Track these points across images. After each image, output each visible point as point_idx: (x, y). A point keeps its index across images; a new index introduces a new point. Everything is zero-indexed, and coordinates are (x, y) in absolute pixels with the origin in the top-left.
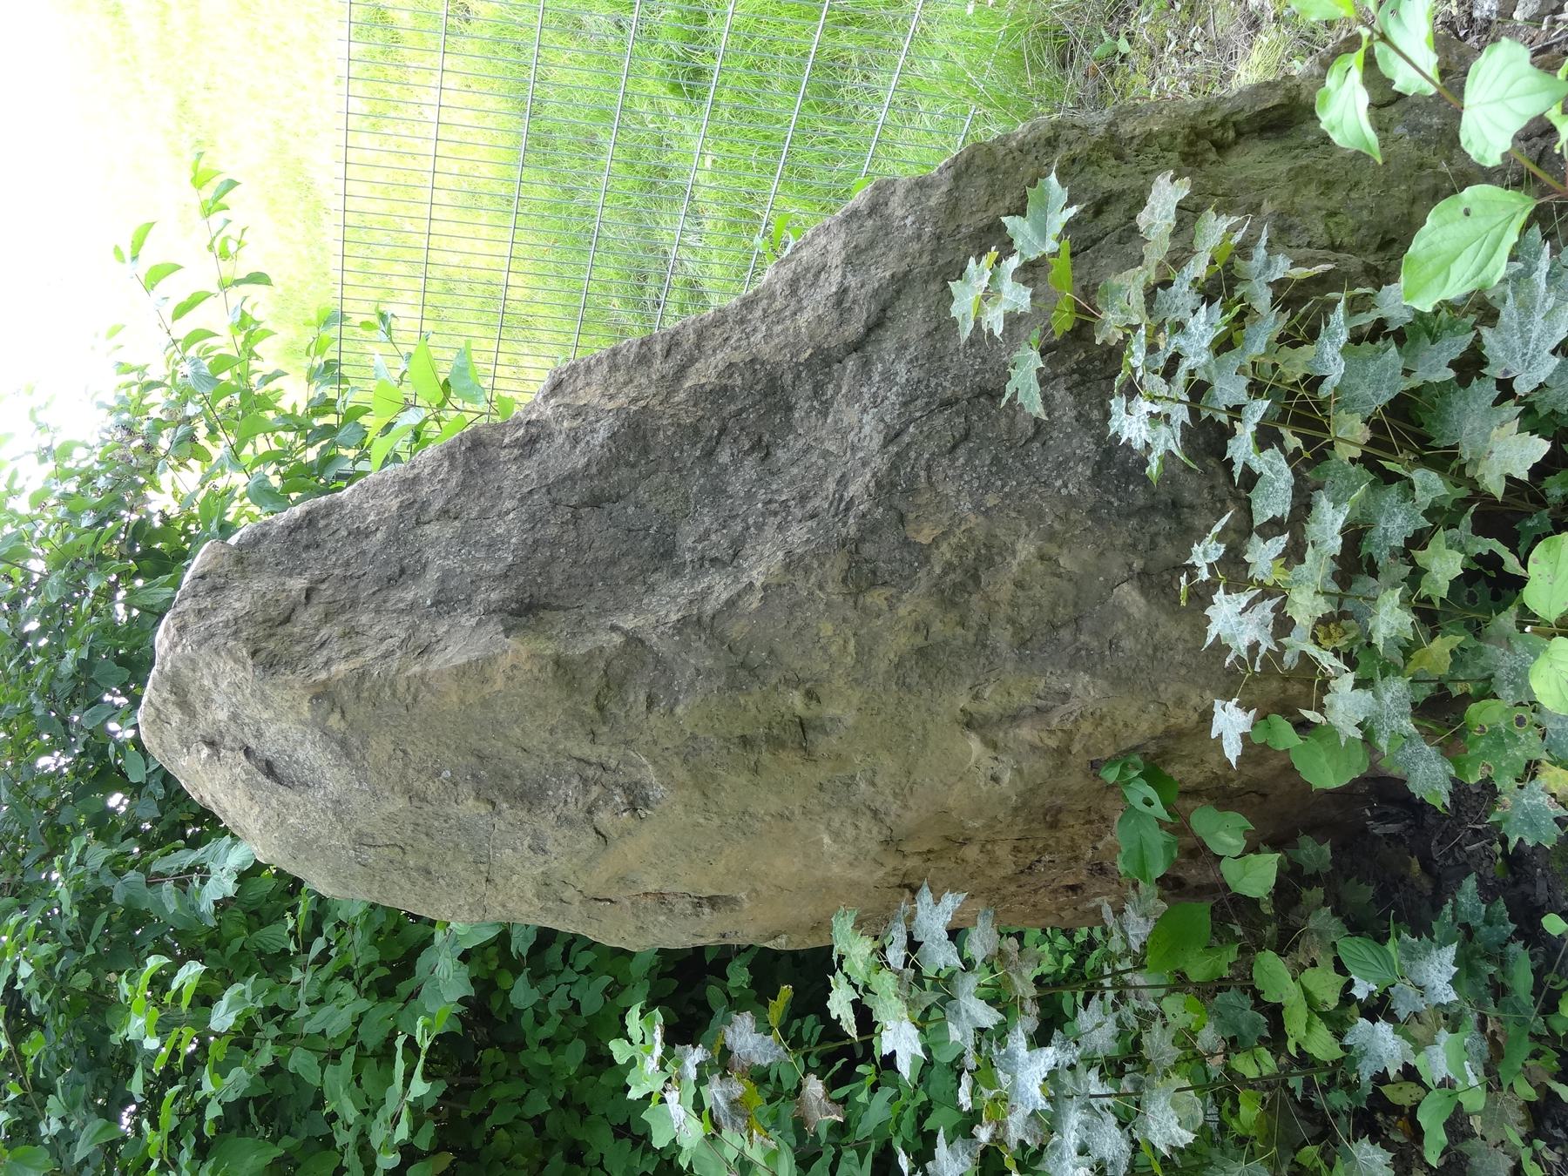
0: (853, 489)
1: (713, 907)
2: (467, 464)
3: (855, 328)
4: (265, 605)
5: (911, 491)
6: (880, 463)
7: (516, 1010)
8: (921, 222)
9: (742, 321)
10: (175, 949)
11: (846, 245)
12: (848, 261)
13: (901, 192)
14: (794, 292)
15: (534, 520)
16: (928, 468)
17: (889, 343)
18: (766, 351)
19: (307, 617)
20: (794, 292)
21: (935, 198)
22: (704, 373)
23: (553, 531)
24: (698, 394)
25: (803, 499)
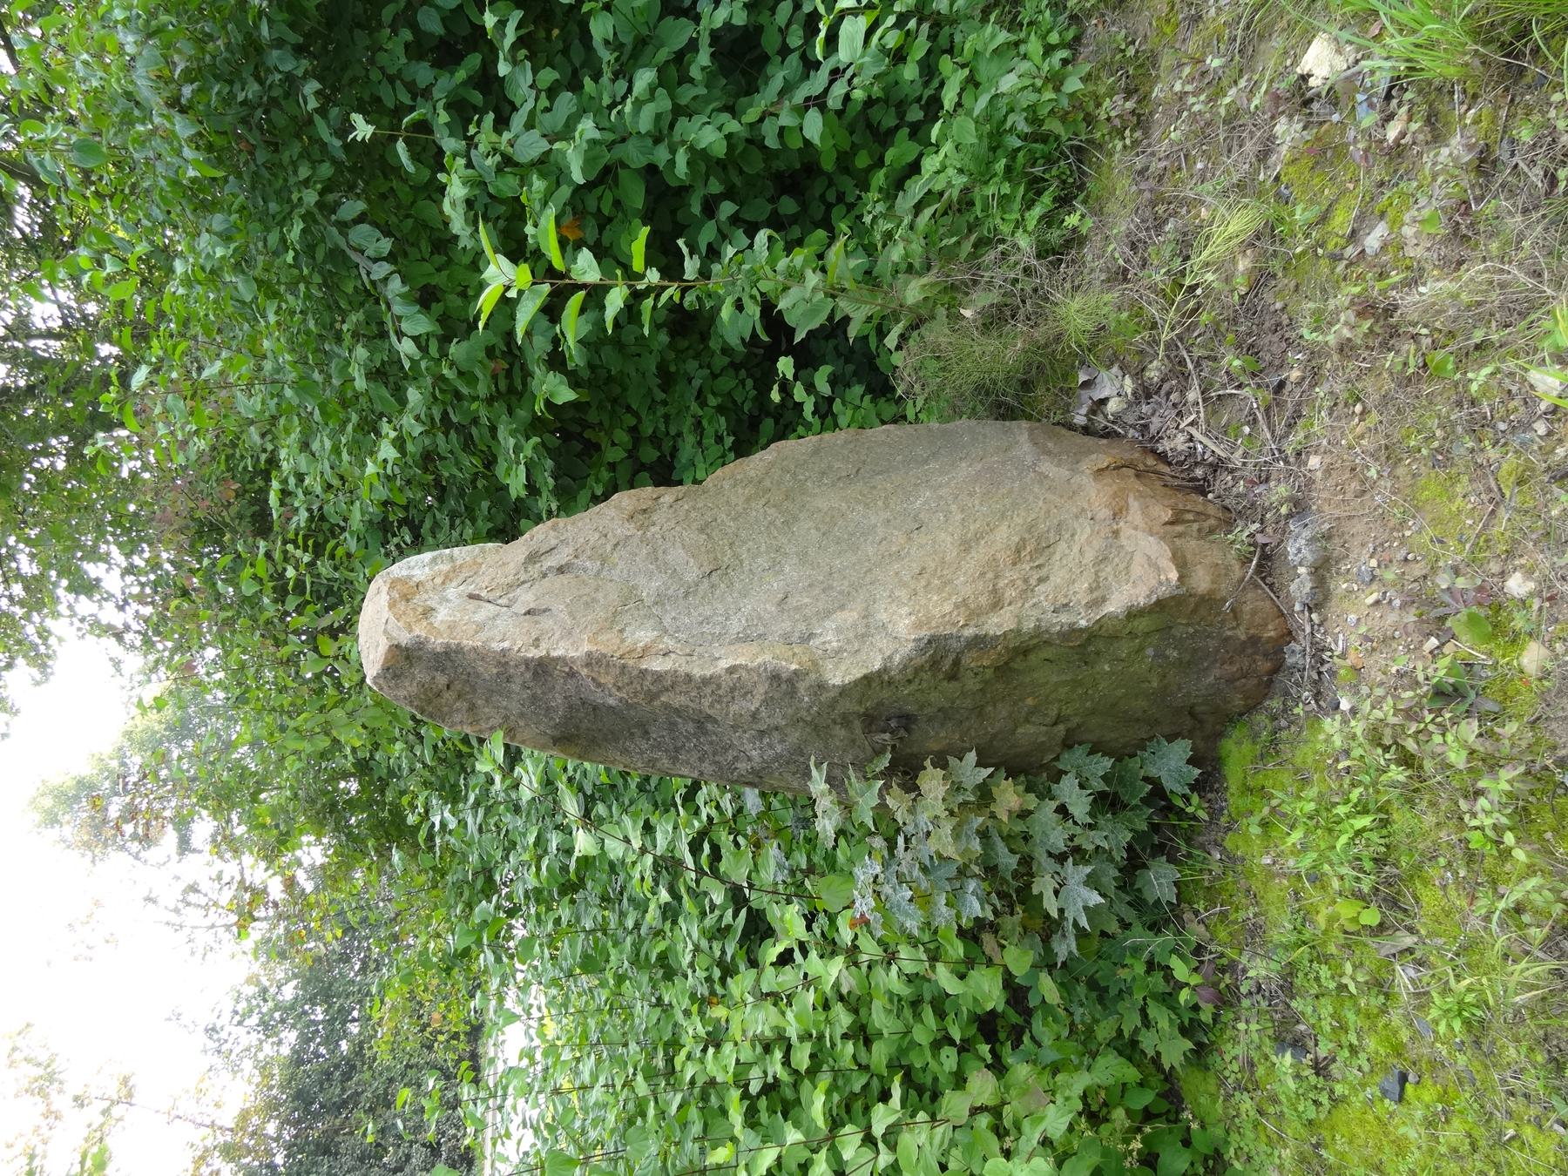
22: (678, 700)
24: (666, 706)
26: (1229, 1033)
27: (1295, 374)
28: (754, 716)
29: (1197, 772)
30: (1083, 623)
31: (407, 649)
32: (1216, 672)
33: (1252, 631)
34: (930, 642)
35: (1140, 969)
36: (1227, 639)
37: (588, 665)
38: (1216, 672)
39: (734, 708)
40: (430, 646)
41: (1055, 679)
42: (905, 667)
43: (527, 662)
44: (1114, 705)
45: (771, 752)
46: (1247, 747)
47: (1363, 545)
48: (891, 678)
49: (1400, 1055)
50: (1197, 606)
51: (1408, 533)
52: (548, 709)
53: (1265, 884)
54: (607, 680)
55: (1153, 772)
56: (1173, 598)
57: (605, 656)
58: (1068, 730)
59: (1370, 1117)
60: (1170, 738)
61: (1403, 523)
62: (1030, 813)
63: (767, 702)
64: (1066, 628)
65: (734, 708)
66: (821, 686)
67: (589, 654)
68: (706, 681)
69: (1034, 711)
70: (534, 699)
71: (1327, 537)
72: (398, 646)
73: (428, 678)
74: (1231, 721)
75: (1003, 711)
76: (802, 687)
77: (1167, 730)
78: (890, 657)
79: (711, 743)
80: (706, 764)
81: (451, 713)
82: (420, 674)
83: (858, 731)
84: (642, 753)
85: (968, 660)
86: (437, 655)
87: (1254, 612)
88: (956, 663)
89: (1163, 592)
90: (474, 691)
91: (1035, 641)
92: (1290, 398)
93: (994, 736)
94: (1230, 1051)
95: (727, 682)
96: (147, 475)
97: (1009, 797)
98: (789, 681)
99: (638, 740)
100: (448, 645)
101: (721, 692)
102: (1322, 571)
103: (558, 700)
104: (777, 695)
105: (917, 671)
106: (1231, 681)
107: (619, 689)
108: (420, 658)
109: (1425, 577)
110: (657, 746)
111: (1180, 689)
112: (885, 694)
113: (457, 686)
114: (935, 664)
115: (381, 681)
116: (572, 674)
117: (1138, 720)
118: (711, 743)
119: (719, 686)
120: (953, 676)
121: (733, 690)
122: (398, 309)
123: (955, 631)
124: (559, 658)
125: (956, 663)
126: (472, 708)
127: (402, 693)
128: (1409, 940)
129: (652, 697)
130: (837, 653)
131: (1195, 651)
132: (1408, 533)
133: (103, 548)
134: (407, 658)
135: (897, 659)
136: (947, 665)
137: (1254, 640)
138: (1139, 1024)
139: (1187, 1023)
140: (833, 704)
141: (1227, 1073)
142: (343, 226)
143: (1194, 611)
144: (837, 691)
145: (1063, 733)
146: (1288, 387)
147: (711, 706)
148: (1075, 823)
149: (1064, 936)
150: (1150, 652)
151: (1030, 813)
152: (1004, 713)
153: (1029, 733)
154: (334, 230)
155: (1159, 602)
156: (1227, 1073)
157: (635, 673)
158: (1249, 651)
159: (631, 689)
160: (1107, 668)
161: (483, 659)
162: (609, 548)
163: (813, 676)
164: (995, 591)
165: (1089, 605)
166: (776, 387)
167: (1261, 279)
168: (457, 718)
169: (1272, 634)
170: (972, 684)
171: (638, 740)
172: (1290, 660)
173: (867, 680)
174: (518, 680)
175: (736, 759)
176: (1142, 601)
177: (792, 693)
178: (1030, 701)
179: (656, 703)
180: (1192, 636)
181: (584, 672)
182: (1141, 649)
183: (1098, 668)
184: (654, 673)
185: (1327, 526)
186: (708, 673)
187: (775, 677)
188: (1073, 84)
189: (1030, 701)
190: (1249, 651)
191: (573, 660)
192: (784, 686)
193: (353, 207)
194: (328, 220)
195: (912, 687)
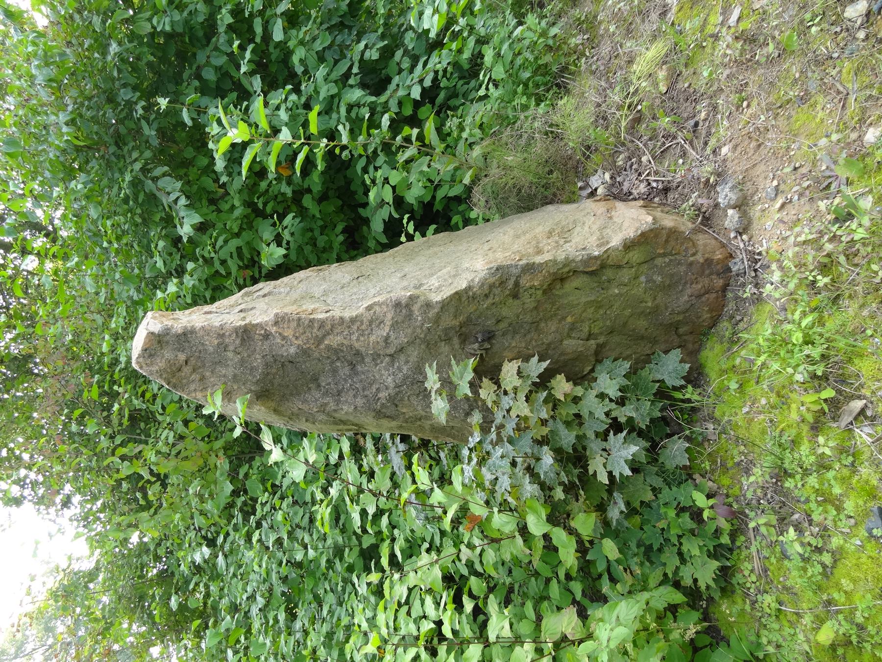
0: (380, 395)
1: (137, 459)
2: (242, 336)
3: (391, 351)
4: (171, 365)
5: (402, 400)
6: (391, 391)
7: (699, 508)
8: (424, 320)
9: (349, 327)
10: (176, 60)
11: (393, 318)
12: (392, 326)
13: (419, 304)
14: (370, 325)
15: (267, 365)
16: (409, 397)
17: (402, 358)
18: (357, 345)
19: (187, 370)
20: (370, 325)
21: (432, 313)
22: (334, 340)
23: (274, 371)
24: (329, 348)
25: (364, 390)
26: (744, 553)
27: (703, 115)
28: (386, 339)
29: (688, 366)
30: (596, 253)
31: (159, 335)
32: (689, 291)
33: (706, 256)
34: (497, 269)
35: (672, 513)
36: (691, 264)
37: (276, 323)
38: (689, 291)
39: (373, 338)
40: (173, 331)
41: (584, 300)
42: (483, 285)
43: (236, 330)
44: (625, 324)
45: (400, 375)
46: (718, 348)
47: (766, 178)
48: (474, 294)
49: (875, 497)
50: (668, 237)
51: (792, 153)
52: (252, 369)
53: (747, 429)
54: (288, 333)
55: (659, 377)
56: (651, 230)
57: (286, 314)
58: (598, 345)
59: (864, 559)
60: (666, 352)
61: (788, 148)
62: (580, 399)
63: (395, 326)
64: (586, 257)
65: (373, 338)
66: (428, 305)
67: (276, 315)
68: (353, 320)
69: (573, 328)
70: (242, 361)
71: (742, 183)
72: (152, 333)
73: (173, 356)
74: (704, 335)
75: (553, 326)
76: (416, 308)
77: (663, 347)
78: (472, 280)
79: (361, 381)
80: (358, 400)
81: (188, 383)
82: (168, 354)
83: (457, 346)
84: (317, 400)
85: (525, 282)
86: (178, 336)
87: (705, 245)
88: (517, 284)
89: (645, 227)
90: (204, 366)
91: (567, 269)
92: (702, 129)
93: (549, 344)
94: (746, 566)
95: (368, 316)
96: (38, 360)
97: (562, 386)
98: (407, 306)
99: (313, 392)
100: (185, 327)
101: (363, 327)
102: (742, 205)
103: (257, 361)
104: (400, 319)
105: (492, 286)
106: (699, 296)
107: (297, 338)
108: (167, 342)
109: (810, 171)
110: (326, 393)
111: (666, 309)
112: (472, 308)
113: (193, 361)
114: (502, 283)
115: (141, 360)
116: (267, 336)
117: (642, 338)
118: (361, 381)
119: (362, 323)
120: (515, 296)
121: (371, 322)
122: (182, 214)
123: (513, 263)
124: (257, 324)
125: (517, 284)
126: (203, 379)
127: (155, 368)
128: (857, 405)
129: (319, 341)
130: (438, 289)
131: (672, 275)
132: (792, 153)
133: (60, 599)
134: (159, 342)
135: (477, 280)
136: (510, 284)
137: (708, 262)
138: (678, 563)
139: (712, 549)
140: (437, 319)
141: (748, 585)
142: (155, 179)
143: (667, 241)
144: (439, 306)
145: (594, 346)
146: (701, 124)
147: (358, 340)
148: (611, 400)
149: (615, 503)
150: (643, 279)
151: (580, 399)
152: (553, 329)
153: (572, 345)
154: (150, 182)
155: (643, 234)
156: (748, 585)
157: (307, 322)
158: (707, 272)
159: (304, 337)
160: (617, 291)
161: (208, 335)
162: (296, 283)
163: (422, 298)
164: (537, 247)
165: (599, 246)
166: (403, 235)
167: (674, 77)
168: (192, 387)
169: (720, 256)
170: (530, 303)
171: (313, 392)
172: (735, 269)
173: (458, 295)
174: (231, 348)
175: (378, 390)
176: (632, 235)
177: (410, 316)
178: (569, 319)
179: (322, 346)
180: (668, 264)
181: (274, 330)
182: (636, 278)
183: (610, 292)
184: (319, 320)
185: (740, 177)
186: (354, 314)
187: (398, 305)
188: (554, 31)
189: (569, 319)
190: (707, 272)
191: (267, 324)
192: (404, 311)
193: (159, 171)
194: (146, 177)
195: (490, 301)
